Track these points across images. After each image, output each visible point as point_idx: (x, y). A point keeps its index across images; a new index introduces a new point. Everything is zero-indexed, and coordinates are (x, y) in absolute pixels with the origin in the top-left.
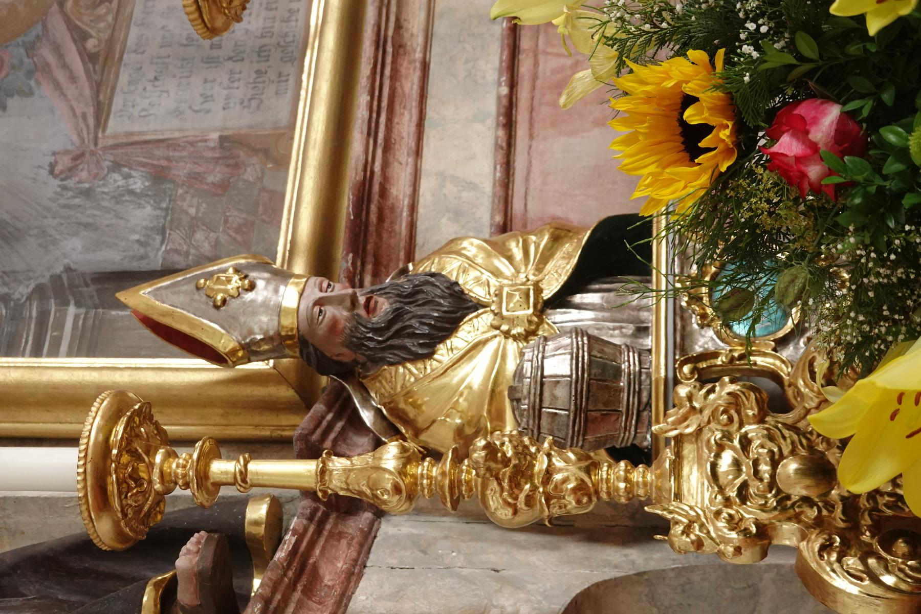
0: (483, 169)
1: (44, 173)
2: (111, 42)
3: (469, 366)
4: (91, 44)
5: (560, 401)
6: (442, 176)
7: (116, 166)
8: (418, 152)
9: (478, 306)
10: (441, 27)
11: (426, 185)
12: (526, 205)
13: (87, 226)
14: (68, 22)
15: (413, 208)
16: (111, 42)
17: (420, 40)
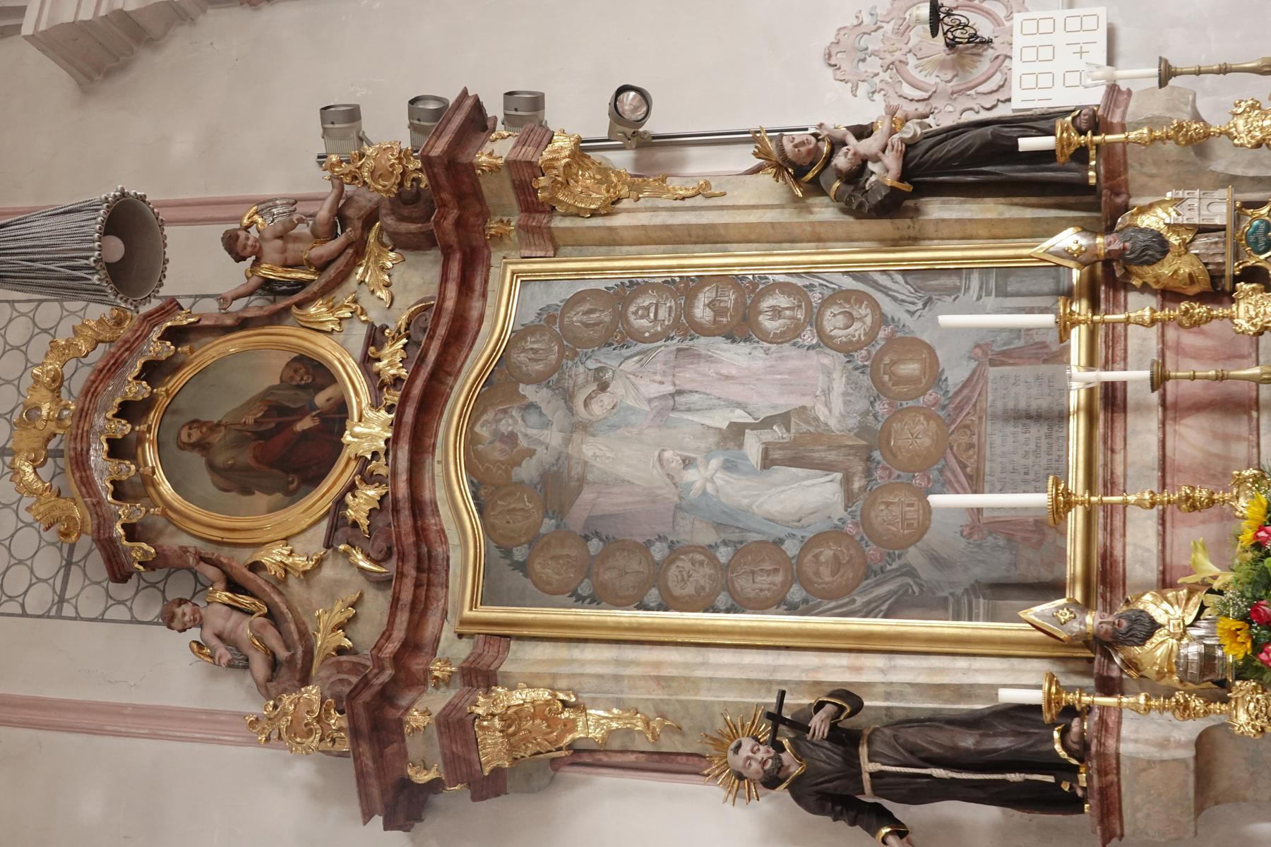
0: (1152, 542)
1: (958, 535)
2: (978, 470)
3: (1157, 650)
4: (968, 470)
5: (1194, 669)
6: (1135, 545)
7: (990, 533)
8: (1124, 535)
9: (1161, 626)
10: (1130, 472)
11: (1129, 549)
12: (1163, 536)
13: (983, 562)
14: (956, 457)
15: (1124, 561)
16: (978, 470)
17: (1122, 480)
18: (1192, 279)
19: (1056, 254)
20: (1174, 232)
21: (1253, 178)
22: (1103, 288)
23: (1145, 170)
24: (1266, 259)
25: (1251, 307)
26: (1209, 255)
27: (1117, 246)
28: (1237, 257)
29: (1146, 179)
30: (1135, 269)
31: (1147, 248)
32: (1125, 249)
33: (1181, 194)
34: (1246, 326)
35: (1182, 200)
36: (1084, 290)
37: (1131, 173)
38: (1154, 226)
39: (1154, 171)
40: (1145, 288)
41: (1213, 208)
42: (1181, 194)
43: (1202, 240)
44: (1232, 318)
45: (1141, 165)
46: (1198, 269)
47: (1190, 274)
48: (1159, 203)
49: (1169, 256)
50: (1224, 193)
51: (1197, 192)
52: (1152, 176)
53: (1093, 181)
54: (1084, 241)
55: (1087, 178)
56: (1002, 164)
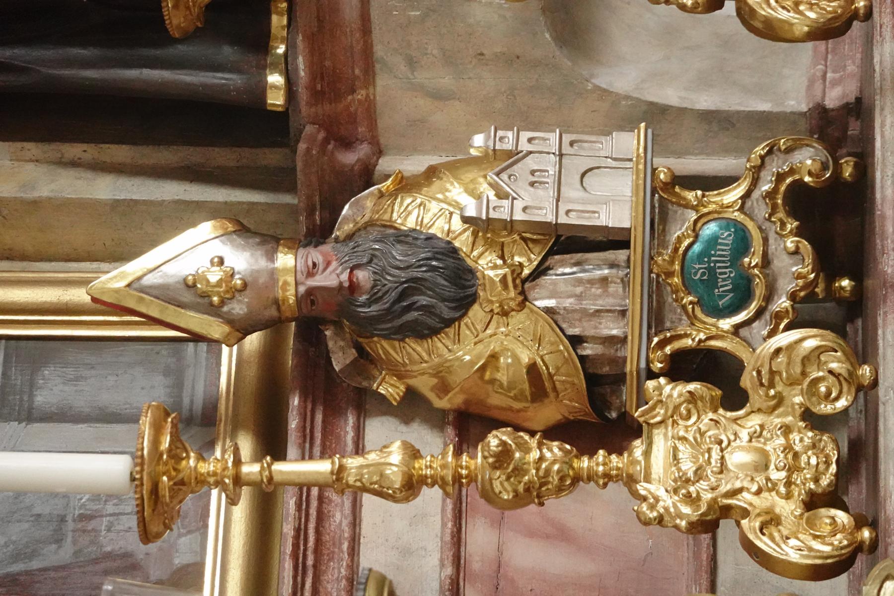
9: (738, 210)
18: (537, 382)
19: (165, 294)
20: (490, 245)
21: (709, 117)
22: (295, 401)
23: (421, 77)
24: (737, 328)
25: (685, 452)
26: (585, 314)
27: (330, 278)
28: (656, 319)
29: (423, 104)
30: (383, 347)
31: (413, 286)
32: (353, 287)
33: (508, 140)
34: (667, 501)
35: (513, 157)
36: (247, 409)
37: (382, 82)
38: (438, 229)
39: (446, 81)
40: (412, 407)
41: (598, 184)
42: (508, 140)
43: (564, 271)
44: (630, 481)
45: (412, 63)
46: (552, 355)
47: (532, 369)
48: (454, 168)
49: (476, 313)
50: (630, 142)
51: (553, 138)
52: (439, 96)
53: (276, 100)
54: (241, 260)
55: (262, 89)
56: (27, 41)
